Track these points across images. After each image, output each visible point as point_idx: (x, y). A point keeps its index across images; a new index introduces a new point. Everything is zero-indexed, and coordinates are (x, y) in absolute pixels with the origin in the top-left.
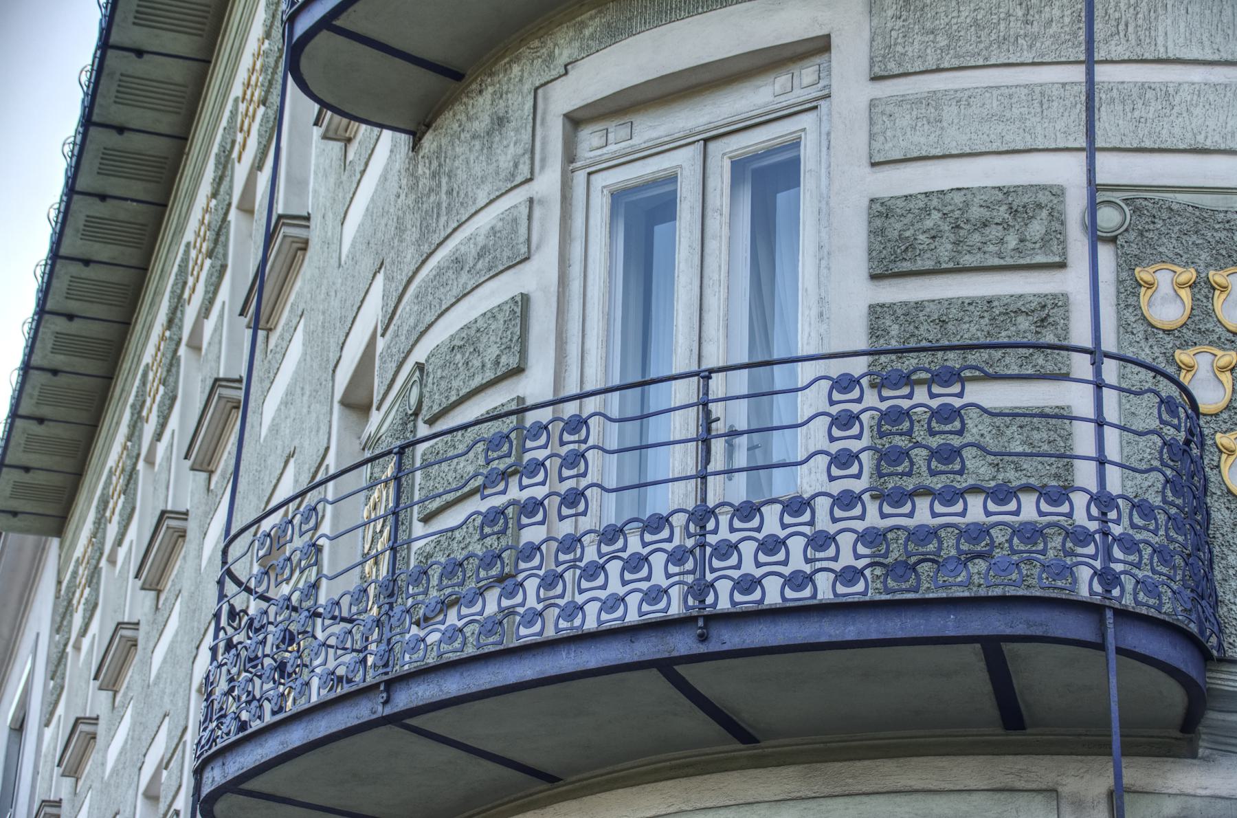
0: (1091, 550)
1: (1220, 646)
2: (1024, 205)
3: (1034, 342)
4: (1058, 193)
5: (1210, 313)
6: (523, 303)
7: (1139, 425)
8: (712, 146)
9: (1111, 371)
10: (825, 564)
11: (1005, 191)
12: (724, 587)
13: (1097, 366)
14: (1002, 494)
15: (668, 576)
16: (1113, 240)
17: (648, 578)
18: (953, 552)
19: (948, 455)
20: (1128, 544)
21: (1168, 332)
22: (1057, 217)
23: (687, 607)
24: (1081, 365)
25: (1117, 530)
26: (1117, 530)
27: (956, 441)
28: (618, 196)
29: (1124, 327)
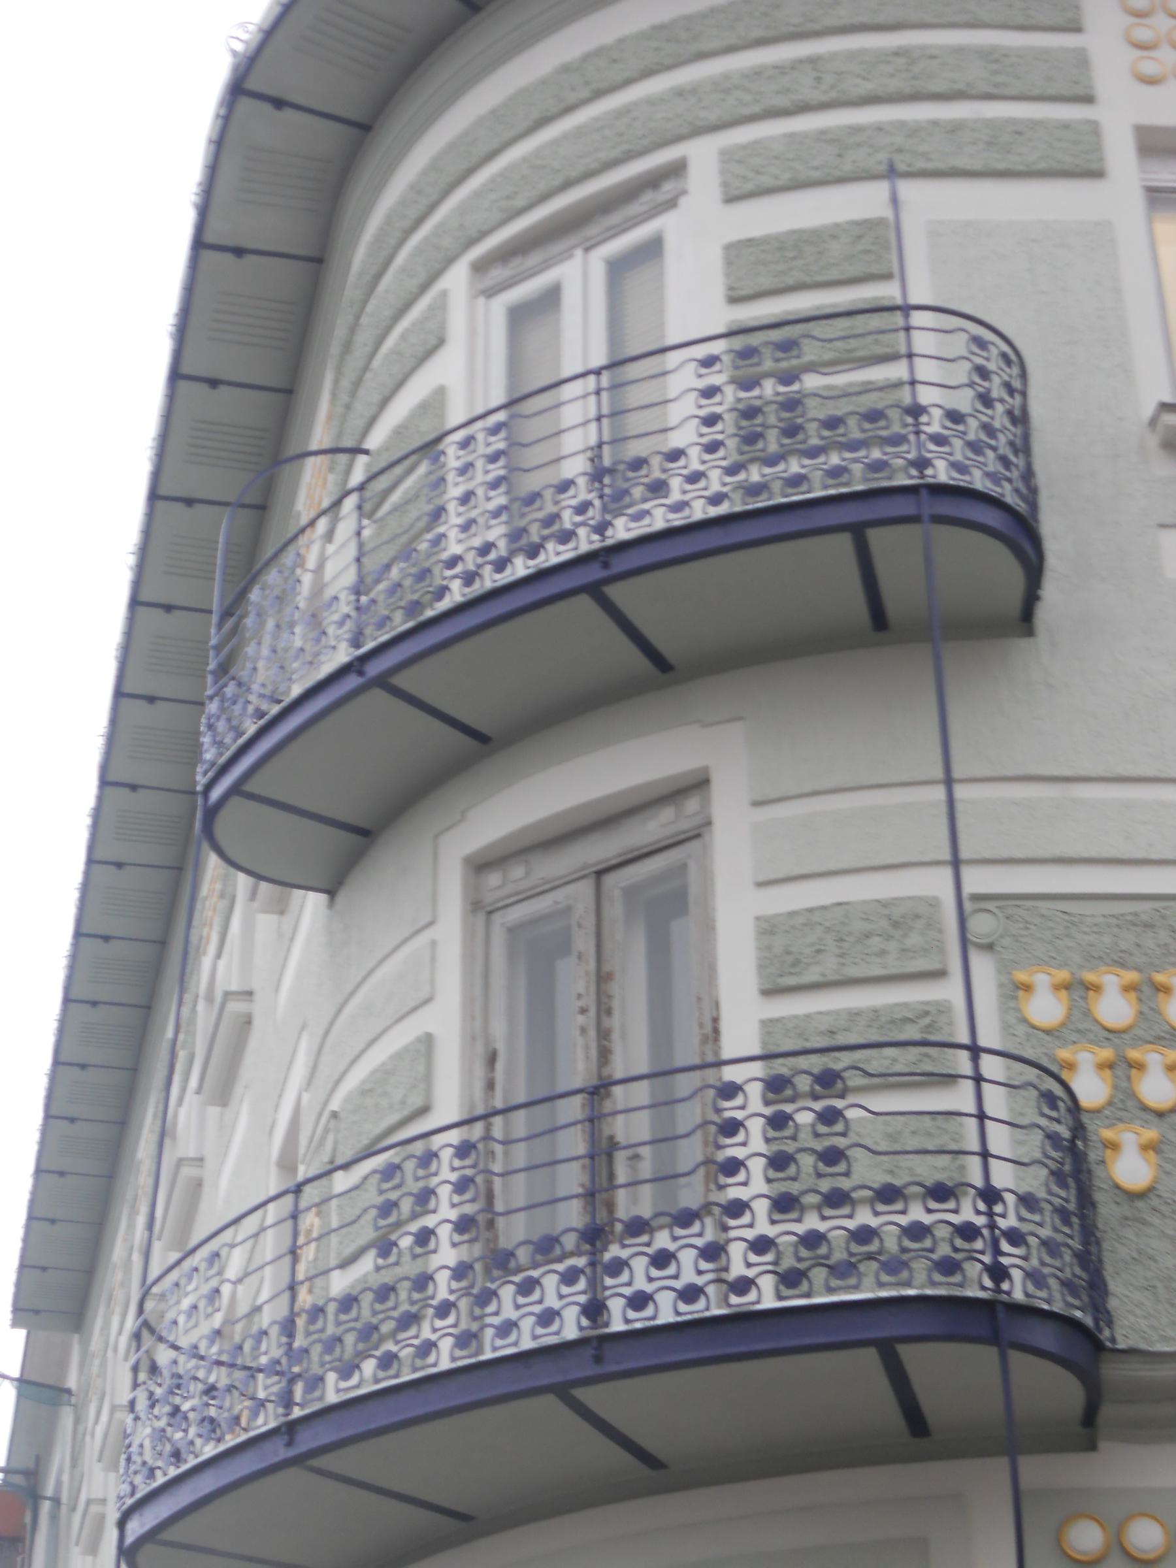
0: (979, 1244)
1: (1113, 1340)
2: (900, 919)
3: (928, 1054)
4: (933, 903)
5: (1087, 1013)
6: (428, 1041)
7: (1024, 1121)
8: (610, 880)
9: (991, 1066)
10: (352, 1325)
11: (884, 904)
12: (616, 1306)
13: (975, 1060)
14: (888, 1195)
15: (561, 1297)
16: (989, 947)
17: (540, 1302)
18: (845, 1256)
19: (832, 1156)
20: (1015, 1238)
21: (1048, 1032)
22: (933, 925)
23: (581, 1328)
24: (962, 1062)
25: (1003, 1223)
26: (1003, 1223)
27: (841, 1142)
28: (513, 931)
29: (1006, 1028)
